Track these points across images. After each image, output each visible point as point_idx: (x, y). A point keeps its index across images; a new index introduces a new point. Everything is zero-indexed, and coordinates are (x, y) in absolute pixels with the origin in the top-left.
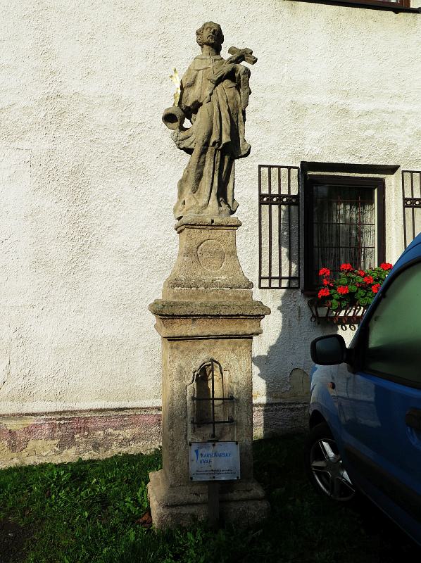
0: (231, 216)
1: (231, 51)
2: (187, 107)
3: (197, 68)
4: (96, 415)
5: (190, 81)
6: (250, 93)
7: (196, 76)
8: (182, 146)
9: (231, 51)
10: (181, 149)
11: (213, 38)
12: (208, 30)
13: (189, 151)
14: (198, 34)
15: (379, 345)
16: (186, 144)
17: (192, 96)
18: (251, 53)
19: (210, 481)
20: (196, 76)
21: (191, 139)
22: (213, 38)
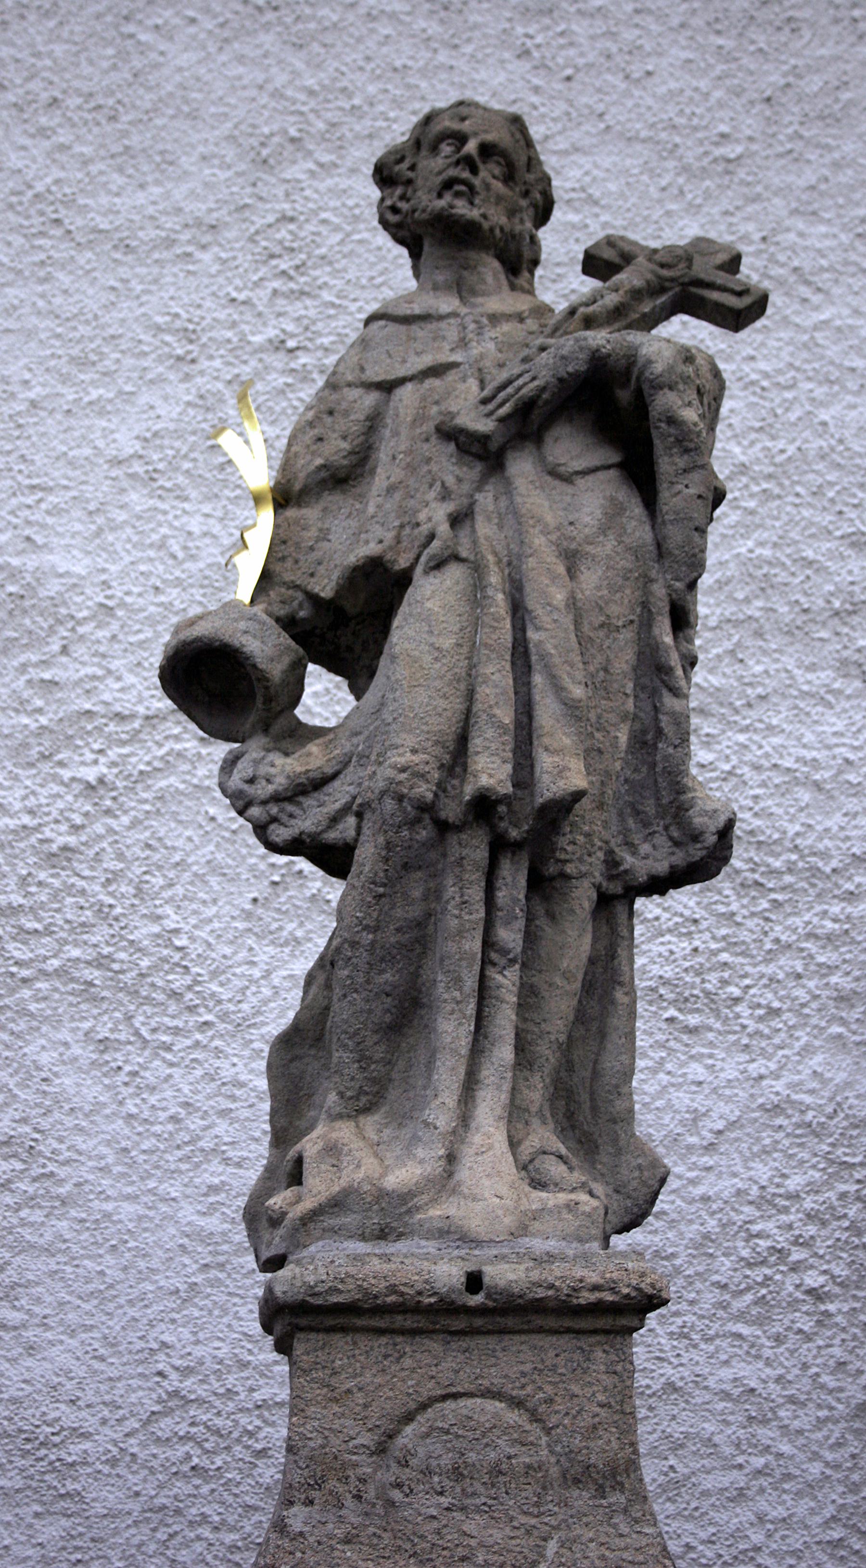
0: (619, 1242)
1: (595, 264)
2: (313, 598)
3: (376, 373)
4: (814, 754)
5: (336, 449)
6: (718, 497)
7: (373, 422)
8: (280, 834)
9: (595, 264)
10: (293, 847)
11: (462, 196)
12: (446, 149)
13: (333, 859)
14: (384, 175)
15: (512, 714)
16: (309, 819)
17: (348, 536)
18: (733, 263)
19: (652, 1202)
20: (373, 422)
21: (339, 794)
22: (462, 196)
